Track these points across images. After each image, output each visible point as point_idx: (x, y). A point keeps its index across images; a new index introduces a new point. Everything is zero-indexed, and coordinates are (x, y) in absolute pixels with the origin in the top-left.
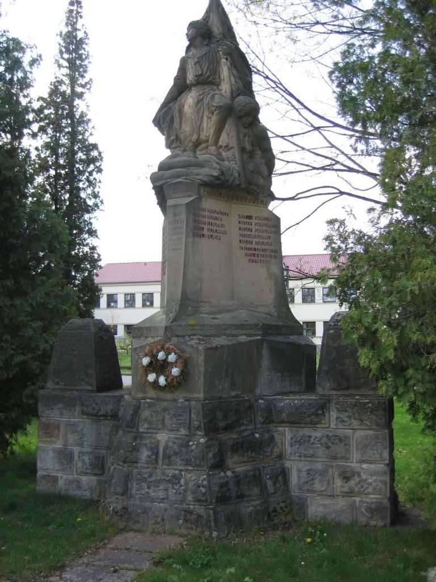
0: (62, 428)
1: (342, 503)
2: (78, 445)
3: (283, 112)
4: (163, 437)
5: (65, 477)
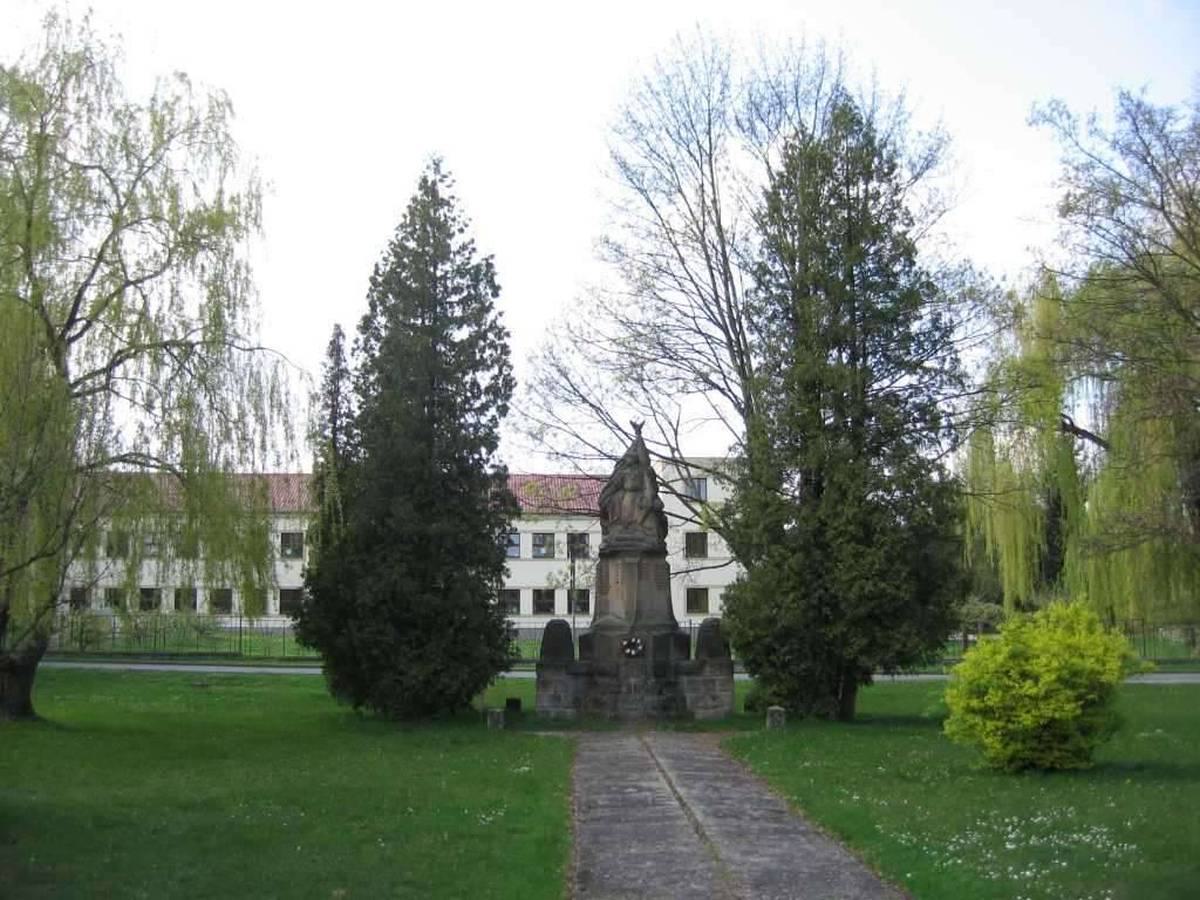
3: (247, 353)
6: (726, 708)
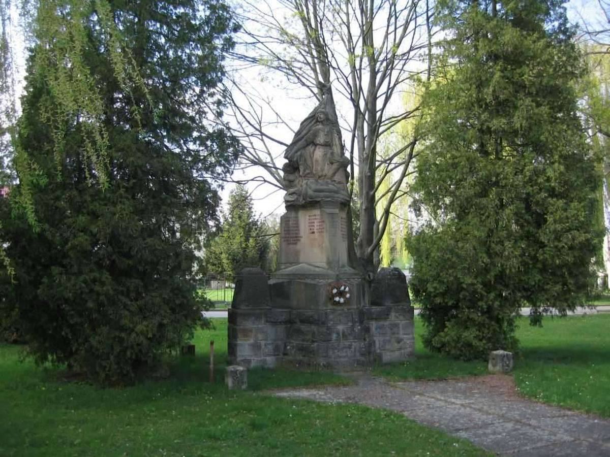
0: (254, 331)
1: (397, 353)
4: (340, 328)
6: (409, 350)
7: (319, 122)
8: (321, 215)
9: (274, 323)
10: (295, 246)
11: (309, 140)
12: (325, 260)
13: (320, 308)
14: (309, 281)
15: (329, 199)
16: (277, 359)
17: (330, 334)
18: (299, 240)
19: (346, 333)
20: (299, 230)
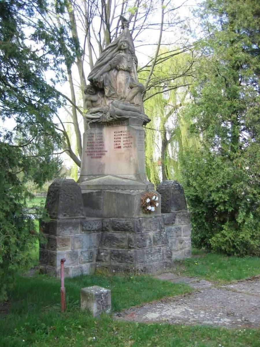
0: (71, 240)
1: (180, 252)
2: (80, 248)
4: (151, 234)
5: (73, 267)
7: (122, 50)
8: (129, 131)
9: (89, 231)
10: (98, 160)
11: (113, 65)
12: (133, 171)
13: (134, 216)
14: (120, 191)
15: (135, 117)
16: (91, 266)
17: (144, 240)
18: (104, 154)
19: (156, 239)
20: (103, 145)
